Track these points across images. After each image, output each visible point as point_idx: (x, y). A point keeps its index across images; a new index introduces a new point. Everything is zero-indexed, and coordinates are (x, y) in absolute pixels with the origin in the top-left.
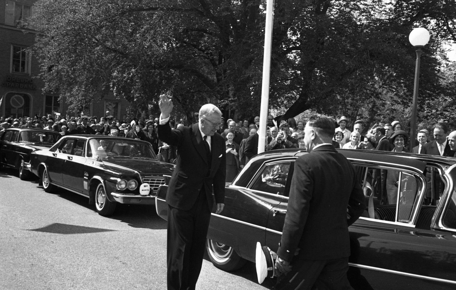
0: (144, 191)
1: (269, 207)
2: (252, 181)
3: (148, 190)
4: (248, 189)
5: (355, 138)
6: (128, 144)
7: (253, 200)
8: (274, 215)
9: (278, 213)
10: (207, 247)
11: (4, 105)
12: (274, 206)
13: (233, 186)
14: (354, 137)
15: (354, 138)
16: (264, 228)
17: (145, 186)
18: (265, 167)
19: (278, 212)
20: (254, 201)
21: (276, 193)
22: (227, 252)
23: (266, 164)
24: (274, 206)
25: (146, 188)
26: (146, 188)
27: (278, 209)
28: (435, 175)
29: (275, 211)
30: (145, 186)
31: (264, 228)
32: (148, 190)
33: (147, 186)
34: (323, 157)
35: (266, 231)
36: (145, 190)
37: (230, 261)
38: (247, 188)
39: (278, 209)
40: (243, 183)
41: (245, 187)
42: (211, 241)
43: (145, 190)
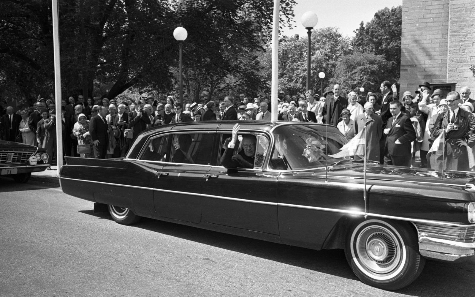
0: (33, 163)
1: (155, 172)
2: (141, 153)
3: (36, 161)
4: (138, 160)
5: (372, 101)
6: (372, 92)
7: (142, 168)
8: (159, 177)
9: (162, 175)
10: (110, 212)
11: (349, 263)
12: (157, 170)
13: (127, 159)
14: (463, 93)
15: (371, 101)
16: (152, 189)
17: (33, 159)
18: (149, 141)
19: (161, 174)
20: (144, 170)
21: (159, 160)
22: (125, 210)
23: (150, 138)
24: (157, 170)
25: (34, 160)
26: (34, 160)
27: (161, 173)
28: (238, 138)
29: (159, 174)
30: (33, 159)
31: (152, 189)
32: (36, 161)
33: (35, 158)
34: (450, 129)
35: (153, 190)
36: (34, 161)
37: (127, 218)
38: (137, 159)
39: (161, 173)
40: (133, 156)
41: (135, 158)
42: (113, 206)
43: (34, 161)
